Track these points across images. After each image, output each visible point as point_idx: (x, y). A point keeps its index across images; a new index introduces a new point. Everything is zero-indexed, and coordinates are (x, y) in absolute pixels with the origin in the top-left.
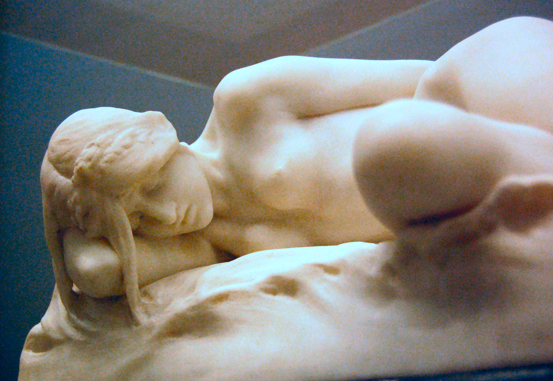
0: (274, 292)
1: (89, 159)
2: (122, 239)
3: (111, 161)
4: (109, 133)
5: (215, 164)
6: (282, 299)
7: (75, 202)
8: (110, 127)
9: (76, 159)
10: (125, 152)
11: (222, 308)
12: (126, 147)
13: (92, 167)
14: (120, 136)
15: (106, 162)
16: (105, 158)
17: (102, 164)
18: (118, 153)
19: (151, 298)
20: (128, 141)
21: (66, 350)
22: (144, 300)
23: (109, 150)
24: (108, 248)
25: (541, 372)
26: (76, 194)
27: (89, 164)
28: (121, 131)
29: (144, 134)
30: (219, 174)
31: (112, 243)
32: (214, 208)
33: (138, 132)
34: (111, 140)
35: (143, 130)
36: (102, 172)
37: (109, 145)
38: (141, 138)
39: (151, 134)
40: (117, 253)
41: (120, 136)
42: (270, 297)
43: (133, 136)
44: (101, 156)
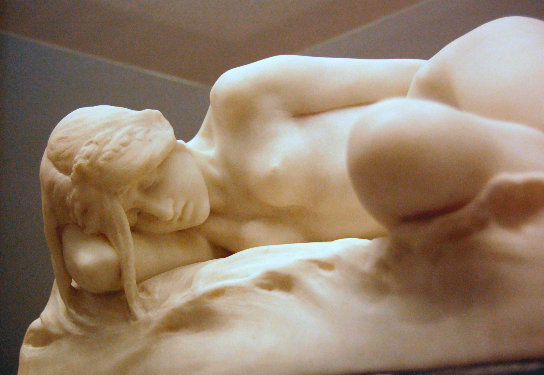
0: (270, 288)
1: (88, 157)
2: (120, 236)
3: (109, 159)
4: (108, 131)
5: (212, 161)
6: (277, 295)
7: (74, 199)
8: (108, 125)
9: (75, 156)
10: (123, 149)
11: (219, 304)
12: (124, 145)
13: (91, 164)
14: (119, 134)
15: (105, 159)
16: (104, 156)
17: (100, 161)
18: (116, 151)
19: (149, 293)
20: (125, 139)
21: (65, 345)
22: (142, 296)
23: (107, 147)
24: (106, 244)
25: (533, 367)
26: (74, 191)
27: (88, 161)
28: (119, 128)
29: (141, 132)
30: (215, 172)
31: (111, 239)
32: (210, 204)
33: (136, 129)
34: (109, 138)
35: (140, 128)
36: (100, 169)
37: (107, 142)
38: (139, 136)
39: (148, 132)
40: (115, 249)
41: (119, 134)
42: (265, 292)
43: (131, 134)
44: (99, 154)
